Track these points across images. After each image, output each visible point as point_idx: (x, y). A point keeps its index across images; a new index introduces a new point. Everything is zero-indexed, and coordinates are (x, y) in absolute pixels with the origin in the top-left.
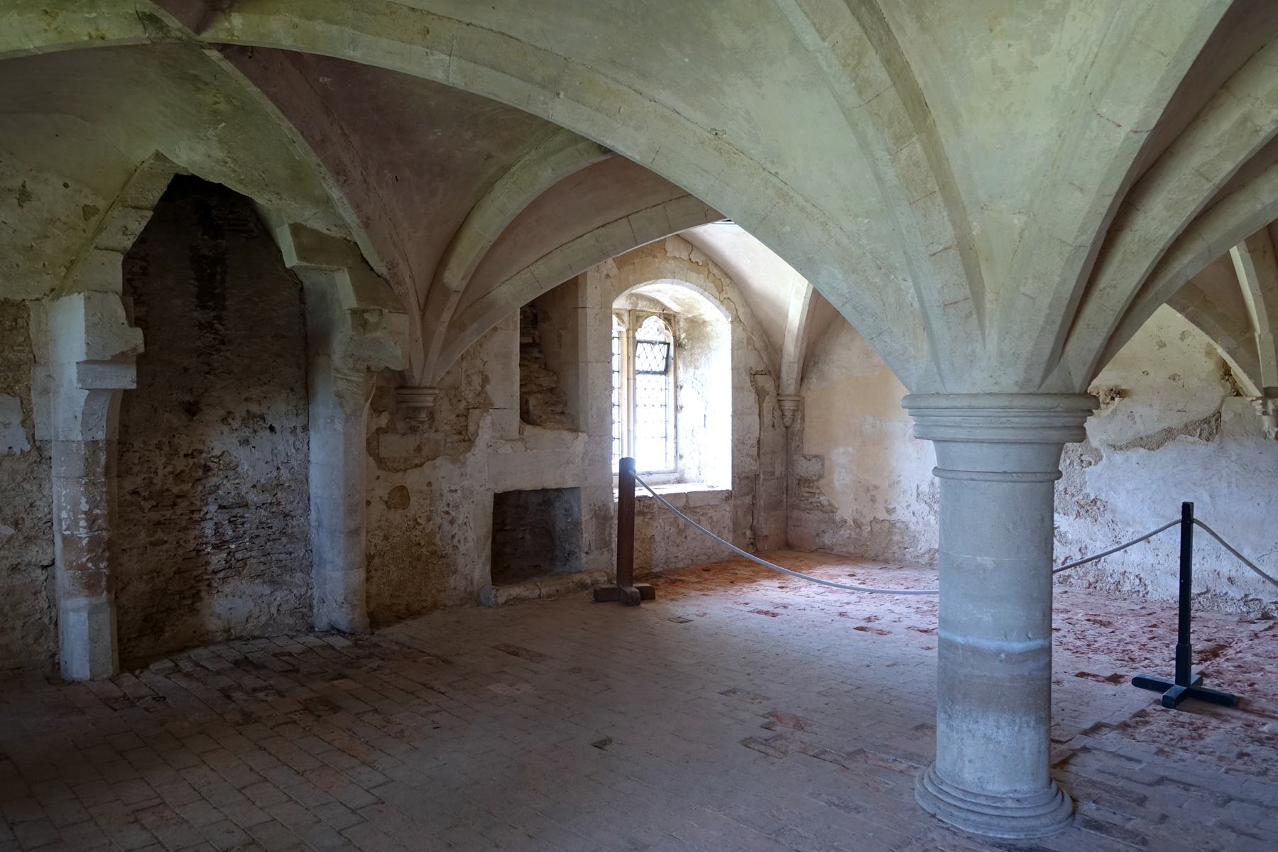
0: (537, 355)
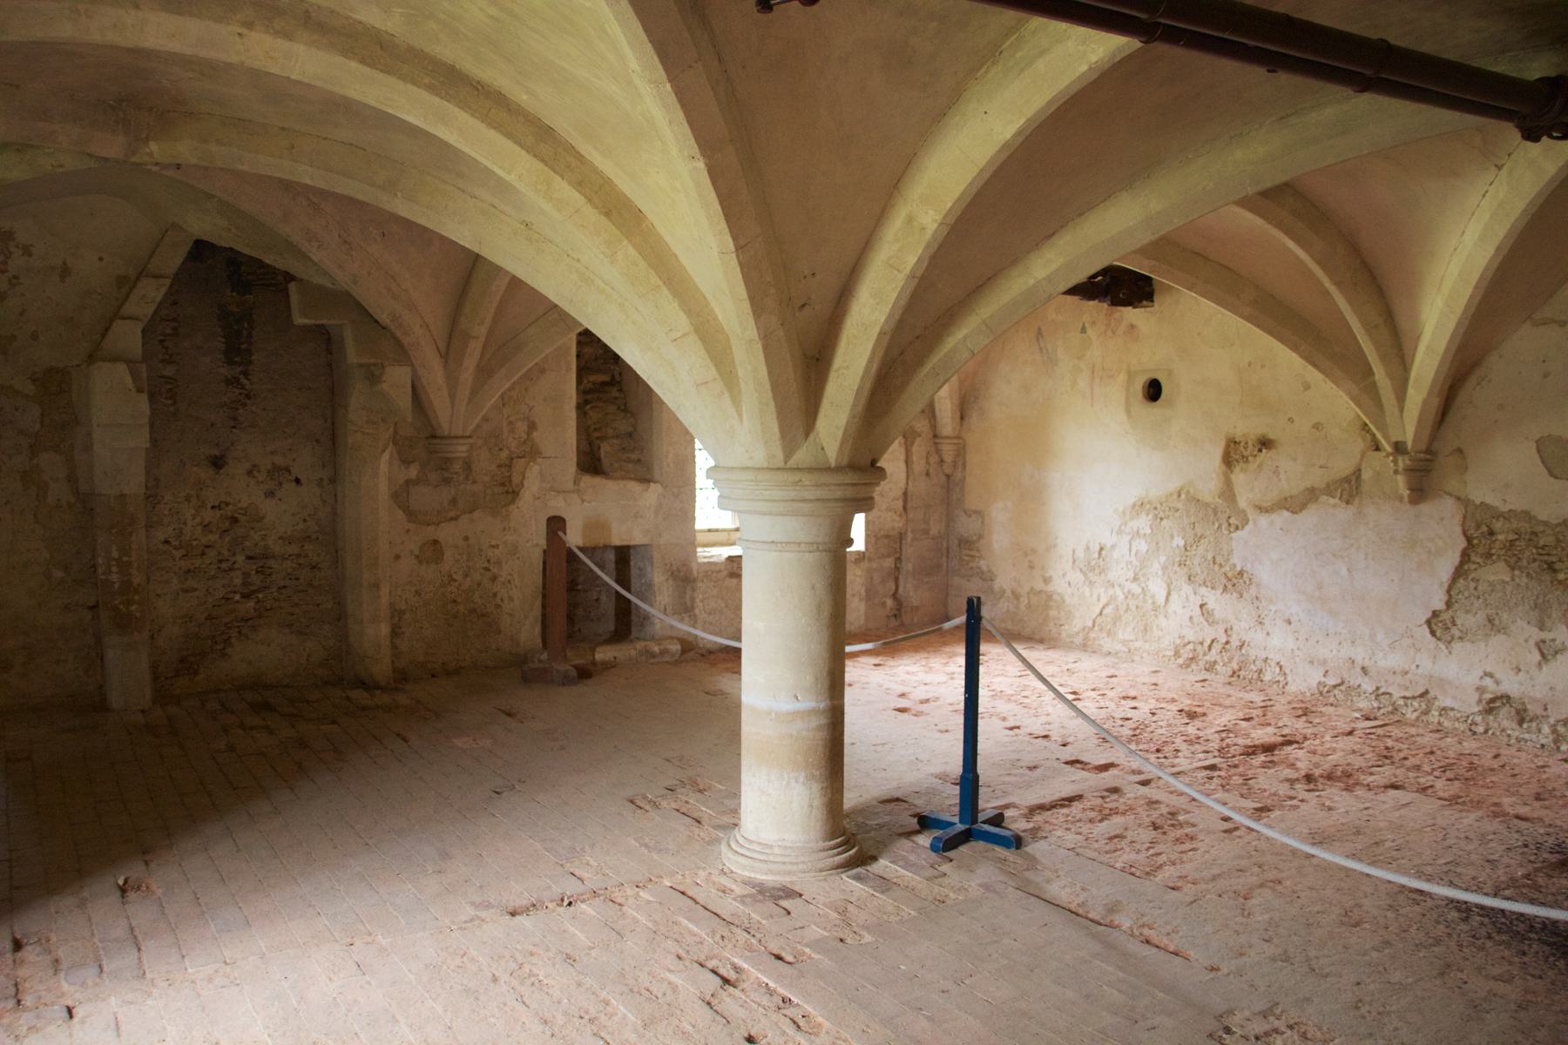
0: (617, 395)
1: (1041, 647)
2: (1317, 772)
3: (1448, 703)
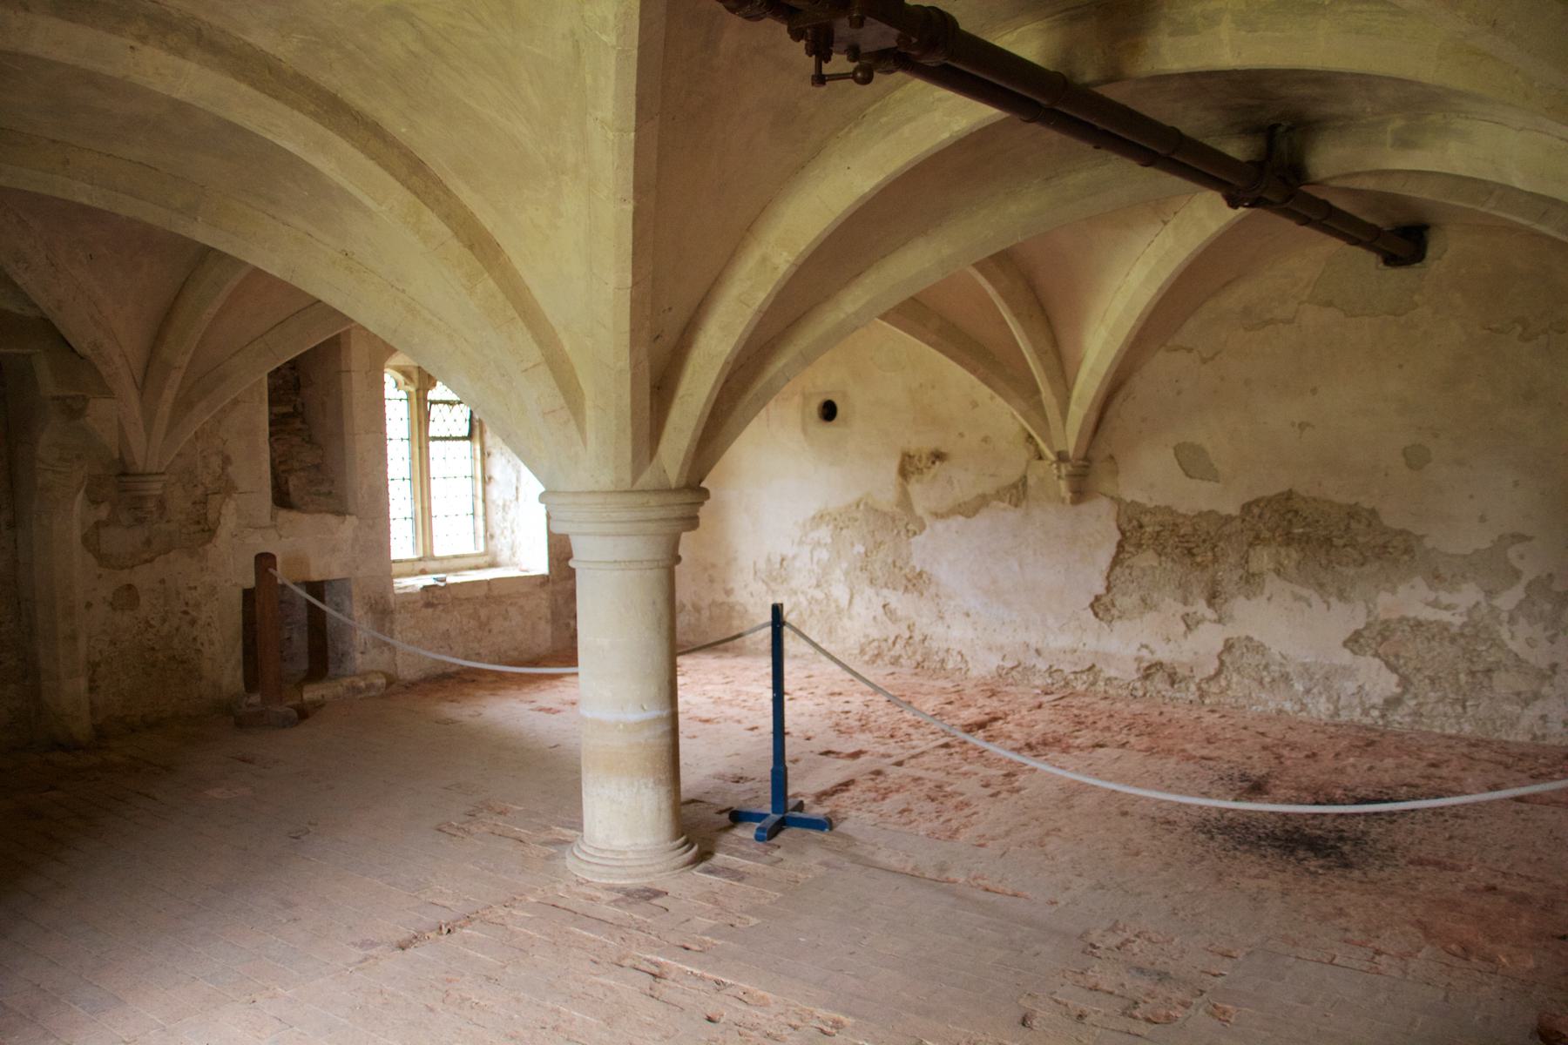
1: (729, 655)
2: (1033, 741)
3: (1112, 673)
